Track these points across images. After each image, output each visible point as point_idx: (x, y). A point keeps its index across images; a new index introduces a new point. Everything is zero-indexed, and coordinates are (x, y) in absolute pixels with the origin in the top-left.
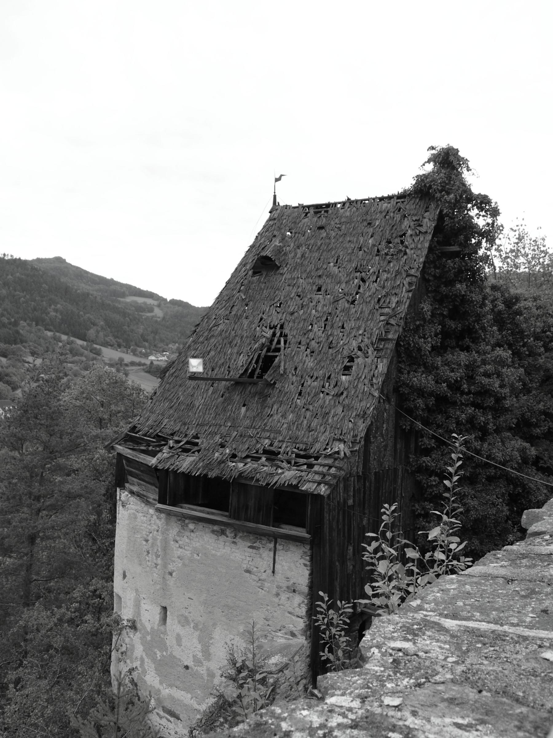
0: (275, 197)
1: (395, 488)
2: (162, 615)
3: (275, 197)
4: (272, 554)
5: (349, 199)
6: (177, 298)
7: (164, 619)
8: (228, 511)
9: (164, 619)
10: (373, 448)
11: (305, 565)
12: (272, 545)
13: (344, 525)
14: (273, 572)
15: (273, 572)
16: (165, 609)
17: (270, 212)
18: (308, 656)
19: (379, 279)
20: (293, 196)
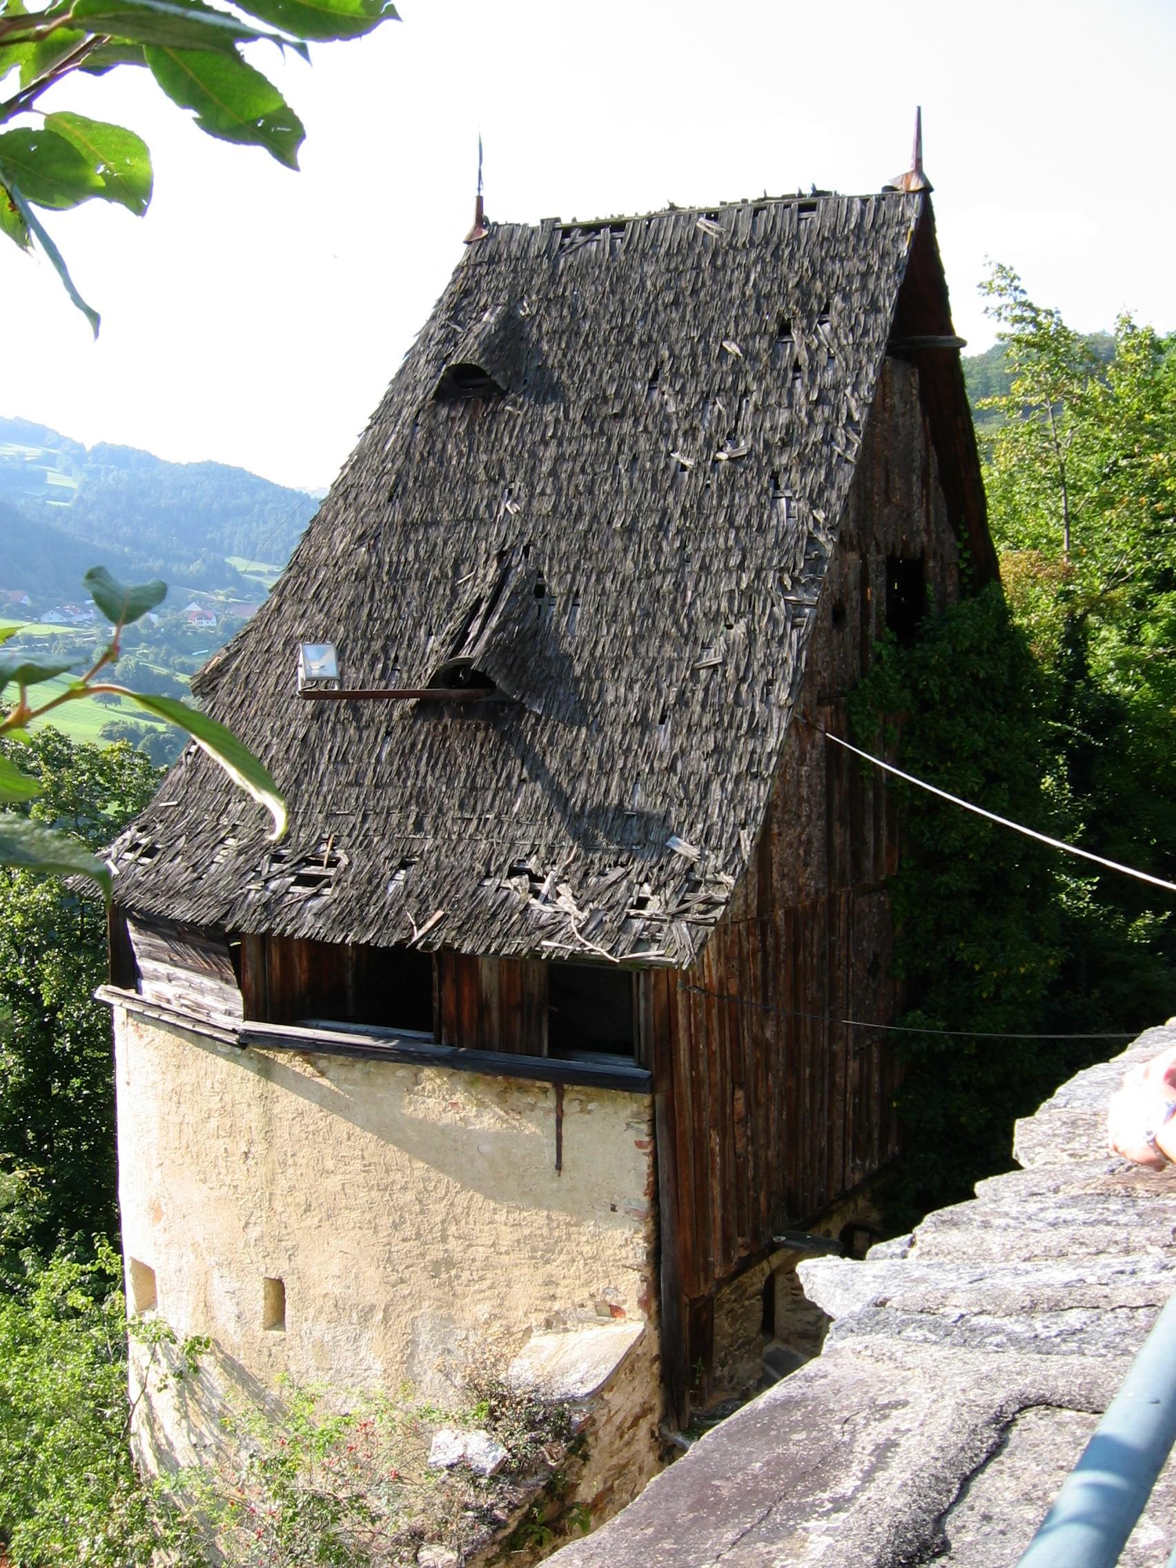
0: (480, 201)
1: (832, 945)
2: (271, 1300)
3: (480, 201)
4: (552, 1121)
5: (673, 208)
6: (117, 438)
7: (277, 1318)
8: (429, 1030)
9: (277, 1318)
10: (777, 852)
11: (639, 1144)
12: (551, 1103)
13: (722, 1043)
14: (559, 1167)
15: (559, 1167)
16: (277, 1288)
17: (468, 242)
18: (657, 1358)
19: (740, 424)
20: (521, 207)
